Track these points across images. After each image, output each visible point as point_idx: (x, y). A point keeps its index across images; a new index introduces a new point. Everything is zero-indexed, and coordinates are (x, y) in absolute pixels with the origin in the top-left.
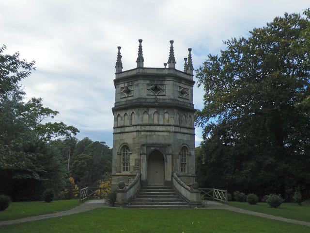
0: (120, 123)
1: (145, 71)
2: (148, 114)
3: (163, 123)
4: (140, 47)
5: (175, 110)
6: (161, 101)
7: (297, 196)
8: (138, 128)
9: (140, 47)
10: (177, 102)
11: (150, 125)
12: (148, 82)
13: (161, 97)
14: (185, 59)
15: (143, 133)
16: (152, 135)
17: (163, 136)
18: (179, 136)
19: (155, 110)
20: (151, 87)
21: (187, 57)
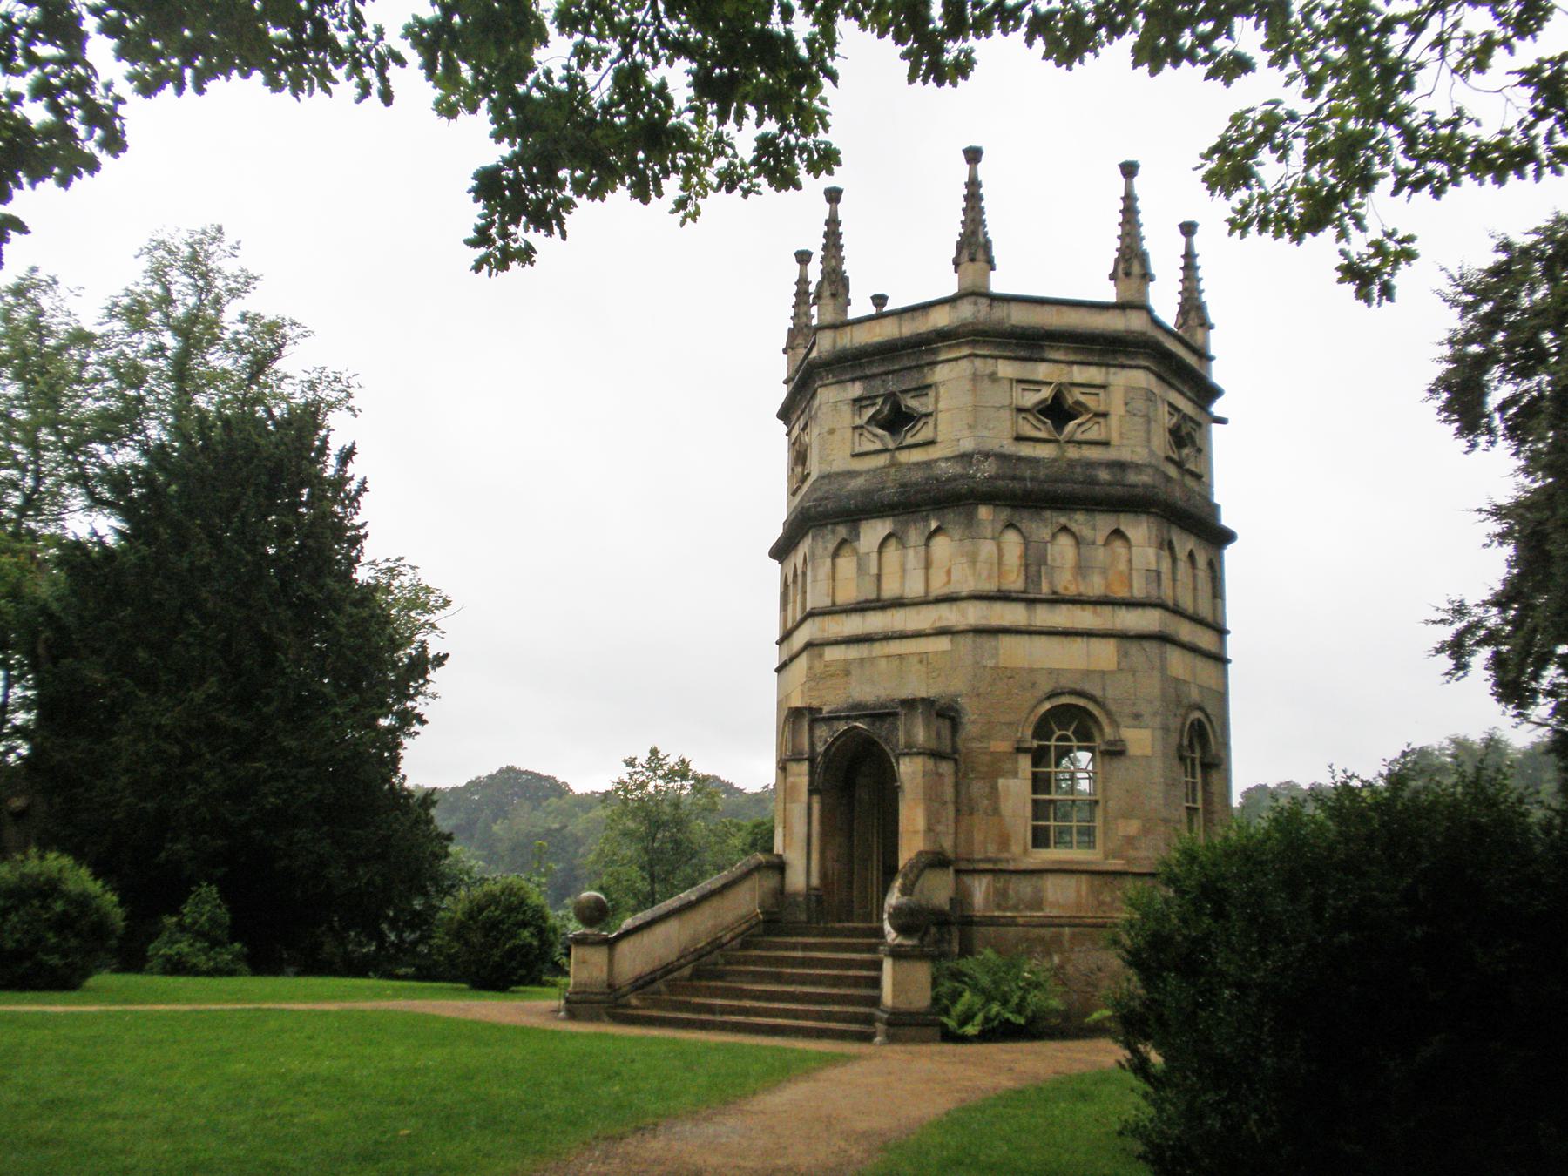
0: (817, 597)
1: (1000, 312)
2: (855, 551)
5: (984, 512)
7: (945, 1119)
8: (974, 614)
10: (858, 483)
12: (856, 390)
14: (803, 257)
15: (832, 654)
17: (923, 658)
18: (1015, 651)
19: (881, 528)
20: (870, 411)
21: (816, 245)
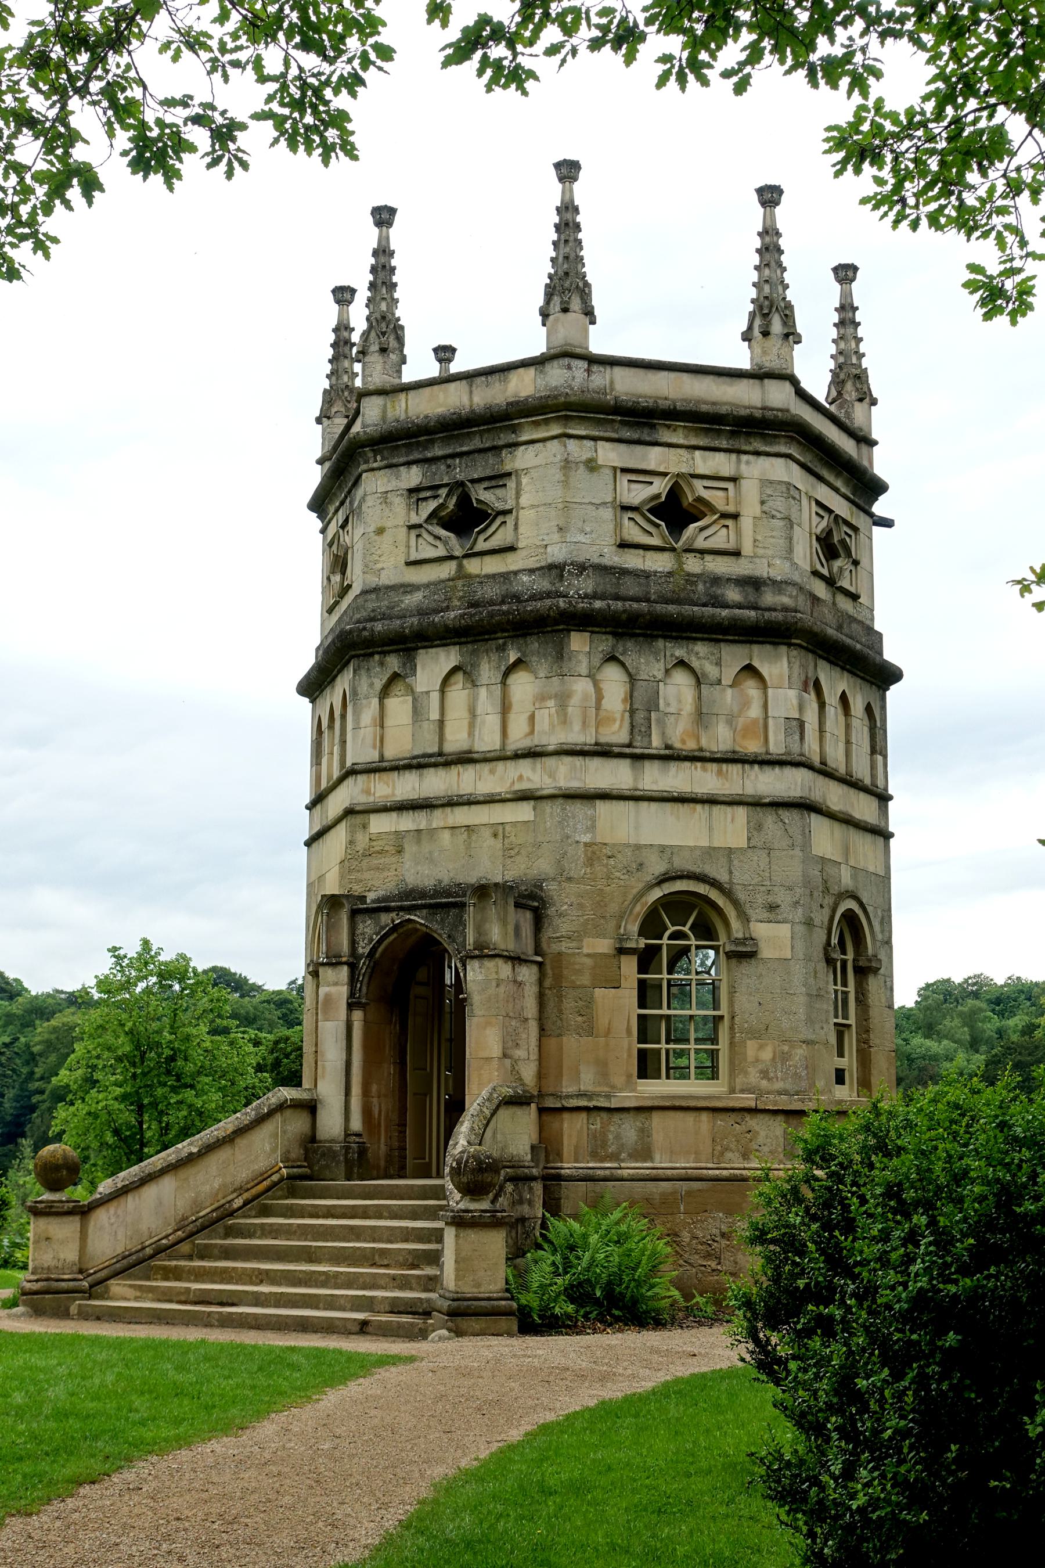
3: (371, 755)
4: (568, 211)
6: (491, 591)
9: (568, 211)
11: (417, 764)
12: (413, 476)
13: (492, 566)
14: (343, 295)
16: (432, 832)
17: (498, 830)
19: (446, 659)
21: (361, 280)
